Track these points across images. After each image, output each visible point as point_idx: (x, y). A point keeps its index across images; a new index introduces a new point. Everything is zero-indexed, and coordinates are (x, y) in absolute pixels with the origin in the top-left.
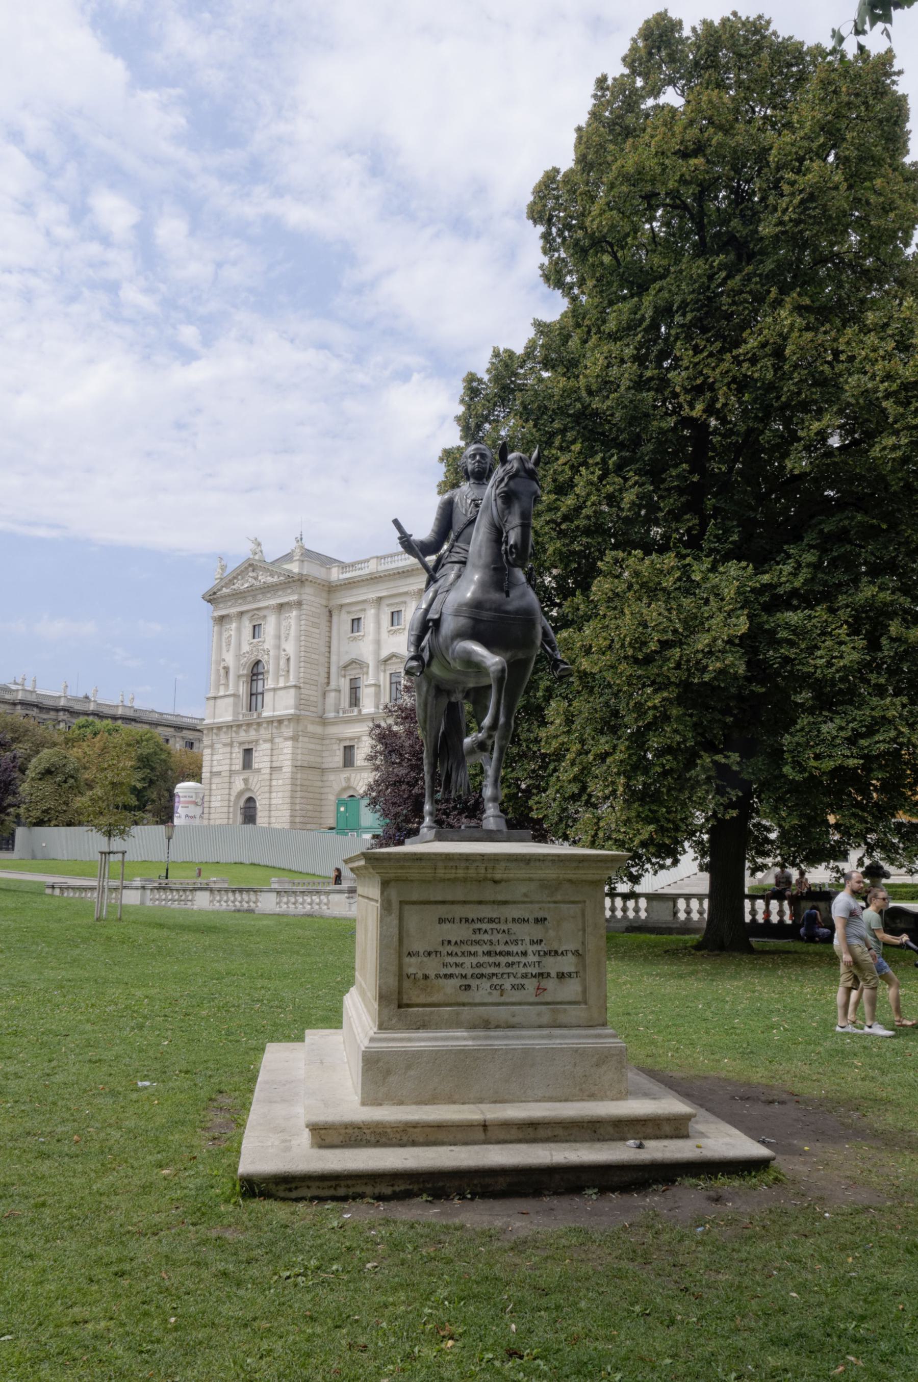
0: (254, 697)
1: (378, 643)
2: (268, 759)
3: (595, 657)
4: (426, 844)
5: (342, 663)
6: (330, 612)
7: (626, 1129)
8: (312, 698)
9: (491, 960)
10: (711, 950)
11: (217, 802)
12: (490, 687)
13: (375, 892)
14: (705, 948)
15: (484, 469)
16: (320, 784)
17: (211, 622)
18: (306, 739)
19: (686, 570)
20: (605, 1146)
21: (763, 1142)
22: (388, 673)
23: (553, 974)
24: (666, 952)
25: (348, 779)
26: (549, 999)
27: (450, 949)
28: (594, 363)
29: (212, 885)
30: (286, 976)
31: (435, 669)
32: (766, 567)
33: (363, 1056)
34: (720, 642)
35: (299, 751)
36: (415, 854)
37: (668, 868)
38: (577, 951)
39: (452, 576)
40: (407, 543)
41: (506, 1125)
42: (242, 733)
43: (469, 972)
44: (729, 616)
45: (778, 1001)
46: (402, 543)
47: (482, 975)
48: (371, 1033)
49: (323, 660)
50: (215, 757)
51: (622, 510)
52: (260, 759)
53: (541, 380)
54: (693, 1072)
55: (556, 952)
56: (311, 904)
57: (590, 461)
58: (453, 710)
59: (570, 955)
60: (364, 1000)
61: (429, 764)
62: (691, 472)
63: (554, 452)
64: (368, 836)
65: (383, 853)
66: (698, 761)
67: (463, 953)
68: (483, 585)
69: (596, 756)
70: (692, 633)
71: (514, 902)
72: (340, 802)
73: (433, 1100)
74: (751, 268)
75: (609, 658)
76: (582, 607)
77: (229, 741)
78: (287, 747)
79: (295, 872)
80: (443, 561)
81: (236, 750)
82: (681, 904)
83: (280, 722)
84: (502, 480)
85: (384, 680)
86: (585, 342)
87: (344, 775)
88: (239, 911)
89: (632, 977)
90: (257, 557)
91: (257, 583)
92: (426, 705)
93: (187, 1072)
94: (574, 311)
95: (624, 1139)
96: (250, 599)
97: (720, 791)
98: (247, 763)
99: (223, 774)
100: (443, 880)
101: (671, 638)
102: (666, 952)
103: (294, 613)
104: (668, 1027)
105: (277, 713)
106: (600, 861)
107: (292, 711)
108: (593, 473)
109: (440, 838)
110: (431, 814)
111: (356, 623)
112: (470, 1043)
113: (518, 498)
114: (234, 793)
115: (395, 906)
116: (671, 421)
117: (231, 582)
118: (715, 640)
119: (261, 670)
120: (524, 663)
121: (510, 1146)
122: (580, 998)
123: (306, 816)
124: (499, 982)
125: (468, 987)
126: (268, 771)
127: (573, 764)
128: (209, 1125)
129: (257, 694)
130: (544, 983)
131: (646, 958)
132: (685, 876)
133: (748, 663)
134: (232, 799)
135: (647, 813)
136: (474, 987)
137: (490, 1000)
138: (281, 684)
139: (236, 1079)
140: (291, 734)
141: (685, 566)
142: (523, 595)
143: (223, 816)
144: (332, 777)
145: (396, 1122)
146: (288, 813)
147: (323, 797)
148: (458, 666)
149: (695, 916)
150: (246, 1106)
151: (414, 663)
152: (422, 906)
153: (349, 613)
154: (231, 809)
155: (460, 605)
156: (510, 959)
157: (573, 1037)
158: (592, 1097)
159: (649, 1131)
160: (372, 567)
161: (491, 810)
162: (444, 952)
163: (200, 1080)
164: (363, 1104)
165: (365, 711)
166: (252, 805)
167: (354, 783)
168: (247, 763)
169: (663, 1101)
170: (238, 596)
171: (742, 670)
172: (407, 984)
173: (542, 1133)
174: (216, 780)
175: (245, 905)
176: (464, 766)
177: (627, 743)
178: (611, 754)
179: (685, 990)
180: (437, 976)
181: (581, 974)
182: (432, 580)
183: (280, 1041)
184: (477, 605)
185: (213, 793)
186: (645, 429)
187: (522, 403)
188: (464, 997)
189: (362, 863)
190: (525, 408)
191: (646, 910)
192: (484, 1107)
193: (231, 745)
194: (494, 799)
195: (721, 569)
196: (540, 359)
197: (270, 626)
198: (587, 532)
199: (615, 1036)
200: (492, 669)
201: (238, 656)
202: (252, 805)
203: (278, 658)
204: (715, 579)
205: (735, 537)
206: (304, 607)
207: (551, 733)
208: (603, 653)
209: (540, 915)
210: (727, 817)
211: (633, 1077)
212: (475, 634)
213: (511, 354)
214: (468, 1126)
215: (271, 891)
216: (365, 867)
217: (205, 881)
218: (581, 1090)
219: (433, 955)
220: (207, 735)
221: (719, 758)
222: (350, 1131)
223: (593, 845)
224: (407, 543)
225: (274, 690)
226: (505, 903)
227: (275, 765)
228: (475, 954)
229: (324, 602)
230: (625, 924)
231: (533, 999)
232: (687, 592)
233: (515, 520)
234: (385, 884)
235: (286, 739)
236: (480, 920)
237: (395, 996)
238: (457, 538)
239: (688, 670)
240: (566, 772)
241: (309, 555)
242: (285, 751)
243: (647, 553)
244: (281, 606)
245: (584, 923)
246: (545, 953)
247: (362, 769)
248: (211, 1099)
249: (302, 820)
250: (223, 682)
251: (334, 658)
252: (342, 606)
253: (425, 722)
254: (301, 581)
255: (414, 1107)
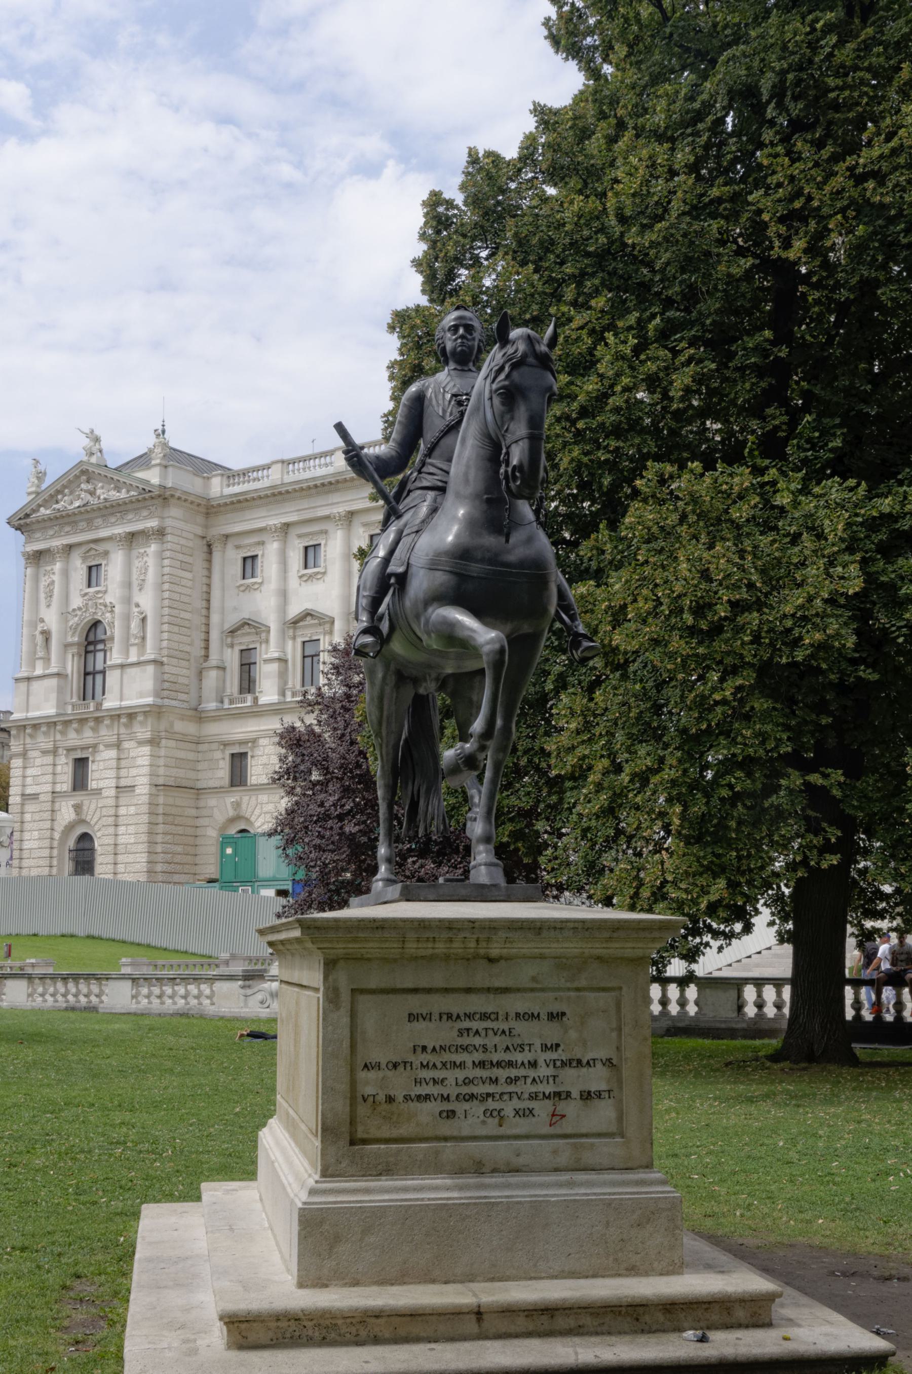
0: (90, 679)
1: (284, 595)
2: (112, 773)
3: (632, 626)
4: (384, 904)
5: (227, 626)
6: (209, 546)
7: (682, 1316)
8: (181, 680)
9: (485, 1074)
10: (796, 1062)
11: (33, 841)
12: (482, 672)
13: (314, 976)
14: (785, 1059)
15: (471, 348)
16: (193, 812)
17: (22, 561)
18: (172, 743)
19: (766, 490)
20: (653, 1339)
21: (878, 1333)
22: (299, 640)
23: (575, 1094)
24: (727, 1065)
25: (237, 805)
26: (569, 1131)
27: (425, 1058)
28: (631, 168)
29: (29, 971)
30: (156, 1105)
31: (397, 646)
32: (883, 488)
33: (300, 1216)
34: (818, 601)
35: (161, 762)
36: (374, 920)
37: (738, 936)
38: (609, 1060)
39: (424, 510)
40: (354, 454)
41: (509, 1311)
42: (72, 734)
43: (453, 1091)
44: (831, 564)
45: (895, 1135)
46: (349, 460)
47: (472, 1097)
48: (311, 1182)
49: (198, 620)
50: (29, 772)
51: (671, 399)
52: (101, 774)
53: (545, 200)
54: (772, 1238)
55: (579, 1062)
56: (185, 997)
57: (620, 324)
58: (420, 704)
59: (599, 1065)
60: (294, 1135)
61: (386, 786)
62: (774, 343)
63: (564, 309)
64: (270, 893)
65: (327, 920)
66: (783, 782)
67: (444, 1064)
68: (471, 524)
69: (634, 776)
70: (773, 588)
71: (518, 990)
72: (226, 840)
73: (402, 1278)
74: (870, 31)
75: (653, 628)
76: (608, 547)
77: (50, 746)
78: (141, 756)
79: (155, 948)
80: (410, 486)
81: (62, 760)
82: (750, 993)
83: (131, 716)
84: (501, 369)
85: (293, 651)
86: (612, 140)
87: (231, 799)
88: (73, 1009)
89: (678, 1101)
90: (94, 460)
91: (93, 501)
92: (381, 698)
93: (23, 1249)
94: (596, 92)
95: (680, 1330)
96: (83, 525)
97: (813, 827)
98: (80, 782)
99: (42, 798)
100: (415, 958)
101: (745, 596)
102: (727, 1065)
103: (153, 548)
104: (734, 1173)
105: (125, 703)
106: (644, 929)
107: (149, 700)
108: (625, 342)
109: (408, 896)
110: (389, 861)
111: (249, 562)
112: (455, 1194)
113: (525, 397)
114: (59, 827)
115: (345, 997)
116: (747, 263)
117: (53, 497)
118: (810, 599)
119: (101, 636)
120: (534, 638)
121: (516, 1342)
122: (613, 1128)
123: (172, 858)
124: (496, 1105)
125: (451, 1114)
126: (113, 792)
127: (599, 788)
128: (66, 1323)
129: (94, 673)
130: (563, 1107)
131: (698, 1075)
132: (759, 951)
133: (857, 632)
134: (57, 836)
135: (710, 858)
136: (460, 1114)
137: (483, 1132)
138: (133, 658)
139: (99, 1257)
140: (148, 735)
141: (762, 485)
142: (530, 540)
143: (41, 862)
144: (212, 802)
145: (350, 1310)
146: (143, 858)
147: (199, 832)
148: (434, 643)
149: (770, 1011)
150: (122, 1296)
151: (369, 639)
152: (384, 997)
153: (238, 547)
154: (55, 852)
155: (438, 554)
156: (513, 1072)
157: (604, 1184)
158: (633, 1271)
159: (715, 1317)
160: (275, 476)
161: (482, 855)
162: (417, 1064)
163: (45, 1261)
164: (301, 1285)
165: (263, 700)
166: (86, 845)
167: (246, 810)
168: (80, 782)
169: (735, 1276)
170: (64, 520)
171: (851, 641)
172: (363, 1110)
173: (562, 1322)
174: (30, 807)
175: (83, 1000)
176: (438, 790)
177: (679, 754)
178: (659, 770)
179: (757, 1119)
180: (407, 1098)
181: (615, 1093)
182: (392, 514)
183: (159, 1201)
184: (462, 554)
185: (27, 826)
186: (707, 276)
187: (516, 235)
188: (446, 1128)
189: (297, 933)
190: (520, 243)
191: (697, 1003)
192: (474, 1286)
193: (54, 752)
194: (487, 840)
195: (817, 490)
196: (544, 167)
197: (114, 568)
198: (617, 432)
199: (664, 1182)
200: (486, 649)
201: (65, 614)
202: (86, 845)
203: (127, 618)
204: (809, 505)
205: (837, 443)
206: (169, 538)
207: (563, 745)
208: (644, 622)
209: (556, 1008)
210: (824, 865)
211: (690, 1243)
212: (458, 596)
213: (494, 157)
214: (454, 1314)
215: (123, 977)
216: (297, 940)
217: (18, 963)
218: (616, 1260)
219: (401, 1068)
220: (17, 737)
221: (815, 778)
222: (283, 1324)
223: (632, 908)
224: (354, 454)
225: (122, 666)
226: (506, 990)
227: (123, 783)
228: (462, 1066)
229: (199, 531)
230: (665, 1024)
231: (546, 1130)
232: (768, 527)
233: (519, 429)
234: (330, 965)
235: (141, 743)
236: (469, 1016)
237: (345, 1129)
238: (430, 452)
239: (772, 644)
240: (586, 803)
241: (176, 458)
242: (140, 761)
243: (709, 466)
244: (132, 538)
245: (619, 1019)
246: (564, 1064)
247: (259, 788)
248: (64, 1287)
249: (165, 867)
250: (40, 654)
251: (215, 618)
252: (227, 537)
253: (380, 723)
254: (162, 497)
255: (375, 1288)
